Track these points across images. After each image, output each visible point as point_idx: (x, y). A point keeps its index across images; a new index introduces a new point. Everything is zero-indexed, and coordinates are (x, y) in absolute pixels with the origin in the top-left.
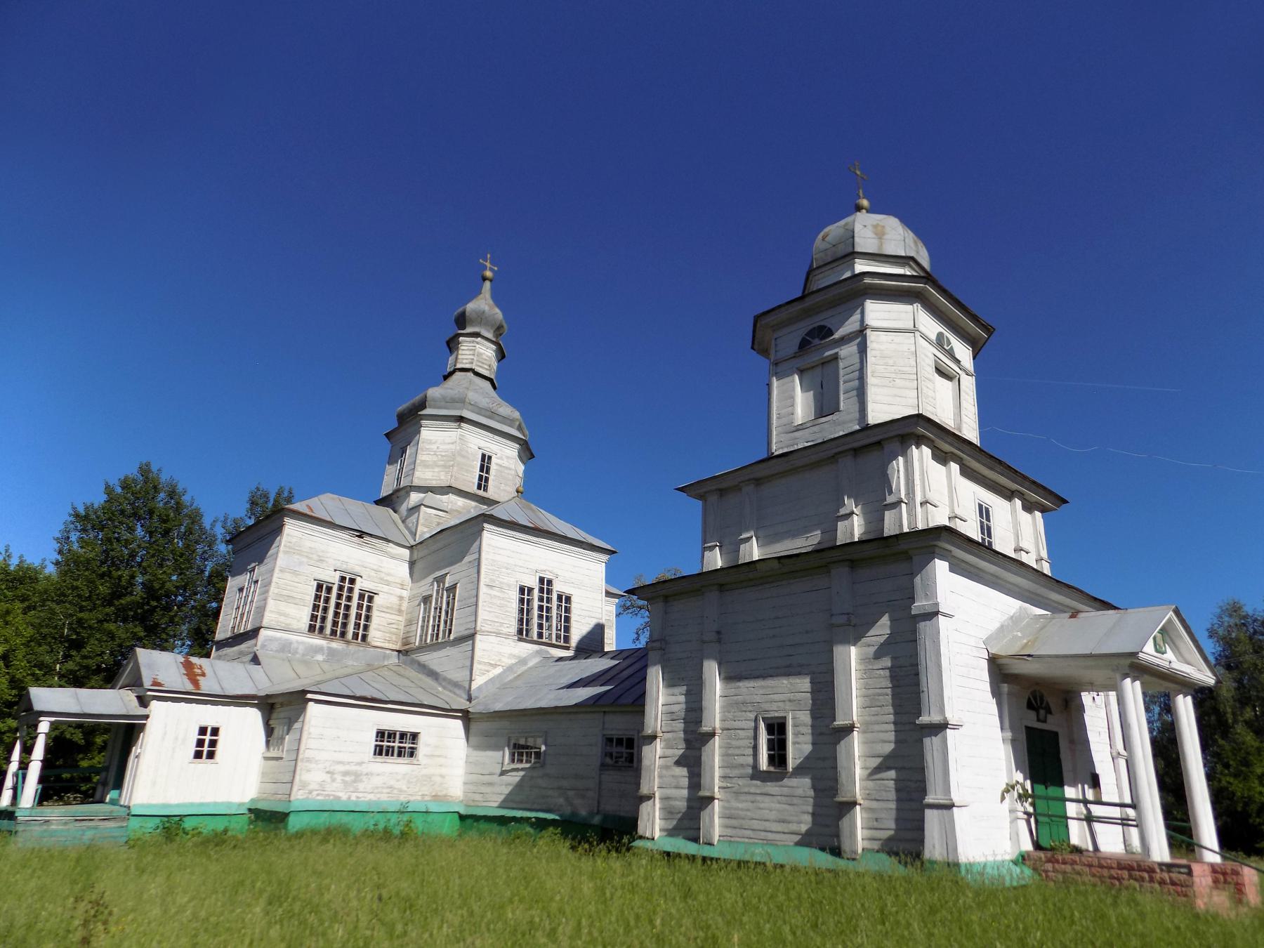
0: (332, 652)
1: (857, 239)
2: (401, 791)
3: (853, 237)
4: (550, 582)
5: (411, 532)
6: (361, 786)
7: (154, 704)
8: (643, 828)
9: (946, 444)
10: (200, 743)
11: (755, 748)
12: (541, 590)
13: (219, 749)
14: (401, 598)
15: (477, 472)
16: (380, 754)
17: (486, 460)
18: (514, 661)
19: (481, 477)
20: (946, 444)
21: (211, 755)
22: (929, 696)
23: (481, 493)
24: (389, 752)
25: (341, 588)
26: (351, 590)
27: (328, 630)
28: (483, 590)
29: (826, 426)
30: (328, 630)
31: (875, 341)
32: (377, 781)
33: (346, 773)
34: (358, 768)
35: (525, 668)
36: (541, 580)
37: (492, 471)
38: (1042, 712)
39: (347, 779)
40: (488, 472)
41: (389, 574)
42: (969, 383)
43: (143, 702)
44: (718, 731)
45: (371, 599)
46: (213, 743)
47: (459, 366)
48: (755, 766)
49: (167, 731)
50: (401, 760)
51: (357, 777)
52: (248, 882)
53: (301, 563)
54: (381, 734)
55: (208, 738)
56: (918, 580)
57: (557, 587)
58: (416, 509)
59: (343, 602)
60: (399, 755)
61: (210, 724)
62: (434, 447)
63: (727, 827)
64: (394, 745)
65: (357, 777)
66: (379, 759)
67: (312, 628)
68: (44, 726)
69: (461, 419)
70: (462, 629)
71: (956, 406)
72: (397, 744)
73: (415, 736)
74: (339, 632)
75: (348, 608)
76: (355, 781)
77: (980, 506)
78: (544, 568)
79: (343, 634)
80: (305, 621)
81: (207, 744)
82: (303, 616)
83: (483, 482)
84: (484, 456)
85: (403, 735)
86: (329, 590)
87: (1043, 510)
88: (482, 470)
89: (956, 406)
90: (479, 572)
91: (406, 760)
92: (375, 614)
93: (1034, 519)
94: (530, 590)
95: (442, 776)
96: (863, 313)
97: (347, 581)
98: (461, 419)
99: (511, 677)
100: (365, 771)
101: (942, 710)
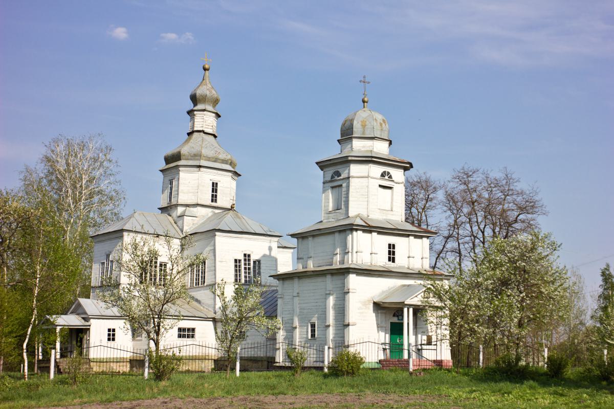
1: (354, 129)
3: (353, 128)
4: (249, 256)
5: (180, 229)
7: (92, 320)
8: (277, 360)
10: (109, 335)
11: (307, 332)
12: (245, 260)
13: (116, 337)
15: (210, 193)
16: (180, 337)
17: (215, 187)
19: (213, 195)
22: (346, 317)
23: (214, 204)
24: (184, 336)
26: (156, 263)
28: (218, 264)
29: (338, 214)
36: (245, 255)
40: (216, 192)
43: (86, 319)
44: (298, 327)
46: (114, 335)
48: (307, 338)
50: (189, 339)
56: (346, 280)
58: (182, 216)
60: (188, 337)
61: (112, 327)
68: (58, 329)
69: (200, 167)
70: (210, 281)
72: (186, 333)
73: (193, 330)
83: (214, 198)
84: (213, 183)
87: (428, 237)
88: (213, 192)
90: (215, 256)
91: (191, 339)
94: (240, 261)
96: (349, 170)
98: (200, 167)
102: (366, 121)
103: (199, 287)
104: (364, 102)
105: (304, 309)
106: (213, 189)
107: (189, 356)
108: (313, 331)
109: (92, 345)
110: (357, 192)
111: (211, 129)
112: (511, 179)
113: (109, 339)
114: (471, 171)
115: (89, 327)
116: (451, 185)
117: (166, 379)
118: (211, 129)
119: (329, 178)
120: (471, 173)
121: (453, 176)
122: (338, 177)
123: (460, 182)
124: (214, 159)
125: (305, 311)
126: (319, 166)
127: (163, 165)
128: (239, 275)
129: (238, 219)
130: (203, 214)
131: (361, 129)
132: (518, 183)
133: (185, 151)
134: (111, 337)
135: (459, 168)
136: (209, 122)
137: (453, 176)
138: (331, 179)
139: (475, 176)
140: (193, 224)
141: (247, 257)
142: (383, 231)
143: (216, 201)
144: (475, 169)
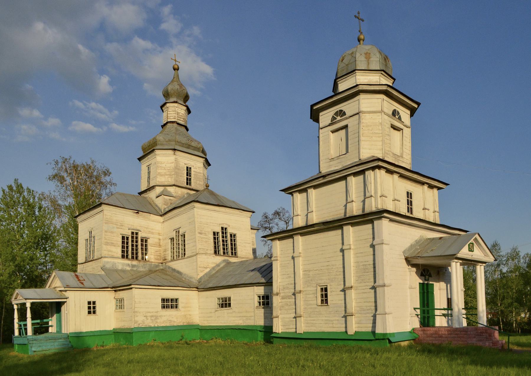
0: (133, 266)
2: (174, 322)
6: (158, 321)
9: (391, 168)
10: (89, 308)
12: (223, 233)
13: (97, 309)
14: (160, 239)
16: (164, 308)
18: (214, 265)
19: (187, 178)
20: (391, 168)
21: (94, 312)
23: (188, 186)
24: (167, 307)
25: (132, 237)
26: (137, 238)
27: (130, 256)
30: (130, 256)
31: (366, 119)
32: (165, 319)
33: (152, 316)
34: (156, 314)
35: (219, 268)
36: (222, 228)
37: (192, 175)
38: (427, 277)
39: (153, 318)
41: (152, 229)
42: (407, 132)
45: (146, 241)
46: (94, 308)
47: (169, 120)
49: (75, 303)
50: (173, 310)
51: (157, 317)
52: (182, 342)
53: (113, 228)
54: (163, 300)
55: (92, 306)
57: (230, 231)
59: (135, 244)
60: (172, 308)
61: (92, 300)
62: (163, 165)
63: (306, 326)
64: (169, 304)
65: (157, 317)
66: (164, 310)
67: (123, 257)
71: (400, 147)
72: (170, 303)
74: (135, 257)
75: (137, 246)
76: (156, 319)
77: (408, 193)
78: (223, 223)
79: (137, 258)
80: (120, 254)
81: (92, 308)
82: (118, 251)
83: (189, 181)
84: (187, 168)
85: (172, 300)
86: (127, 238)
87: (439, 188)
88: (187, 175)
89: (400, 147)
92: (149, 247)
93: (433, 193)
94: (218, 233)
95: (190, 315)
97: (135, 235)
99: (214, 272)
100: (159, 315)
101: (383, 280)
102: (370, 53)
104: (359, 40)
105: (309, 271)
106: (187, 173)
110: (369, 130)
124: (187, 146)
125: (311, 273)
133: (160, 138)
134: (92, 310)
138: (331, 121)
140: (171, 203)
143: (190, 185)
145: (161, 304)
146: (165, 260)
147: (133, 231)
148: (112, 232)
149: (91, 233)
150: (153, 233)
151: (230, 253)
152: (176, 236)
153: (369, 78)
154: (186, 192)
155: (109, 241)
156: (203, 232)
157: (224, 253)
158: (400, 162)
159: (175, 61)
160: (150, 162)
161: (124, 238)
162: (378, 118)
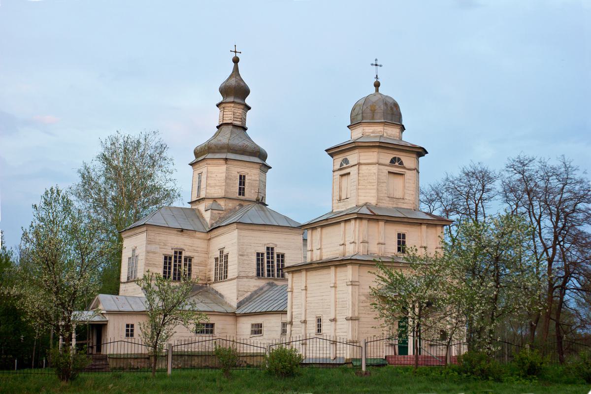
4: (272, 249)
10: (127, 331)
12: (268, 253)
17: (242, 179)
18: (256, 289)
23: (241, 197)
24: (202, 332)
25: (175, 257)
26: (180, 257)
36: (268, 248)
40: (244, 185)
45: (190, 260)
46: (132, 331)
47: (225, 122)
57: (277, 251)
60: (207, 333)
61: (130, 323)
83: (242, 191)
84: (241, 176)
86: (170, 258)
94: (262, 254)
97: (178, 253)
103: (222, 282)
107: (188, 351)
108: (319, 326)
109: (109, 341)
110: (364, 179)
111: (240, 121)
112: (569, 167)
113: (127, 335)
114: (527, 160)
115: (106, 323)
116: (507, 175)
117: (297, 376)
118: (240, 121)
119: (338, 167)
120: (526, 162)
121: (507, 165)
122: (346, 164)
123: (515, 172)
126: (330, 154)
127: (193, 158)
128: (262, 268)
129: (262, 212)
130: (231, 208)
131: (370, 114)
132: (576, 171)
135: (514, 156)
136: (238, 114)
137: (507, 165)
138: (340, 166)
139: (531, 164)
141: (270, 250)
142: (389, 220)
143: (243, 195)
144: (530, 157)
145: (125, 333)
146: (210, 280)
147: (176, 250)
148: (154, 253)
149: (134, 251)
150: (197, 252)
151: (276, 275)
152: (220, 256)
153: (373, 128)
154: (238, 204)
155: (151, 262)
156: (245, 253)
157: (269, 275)
158: (399, 204)
159: (235, 52)
160: (201, 170)
161: (167, 258)
162: (374, 169)
